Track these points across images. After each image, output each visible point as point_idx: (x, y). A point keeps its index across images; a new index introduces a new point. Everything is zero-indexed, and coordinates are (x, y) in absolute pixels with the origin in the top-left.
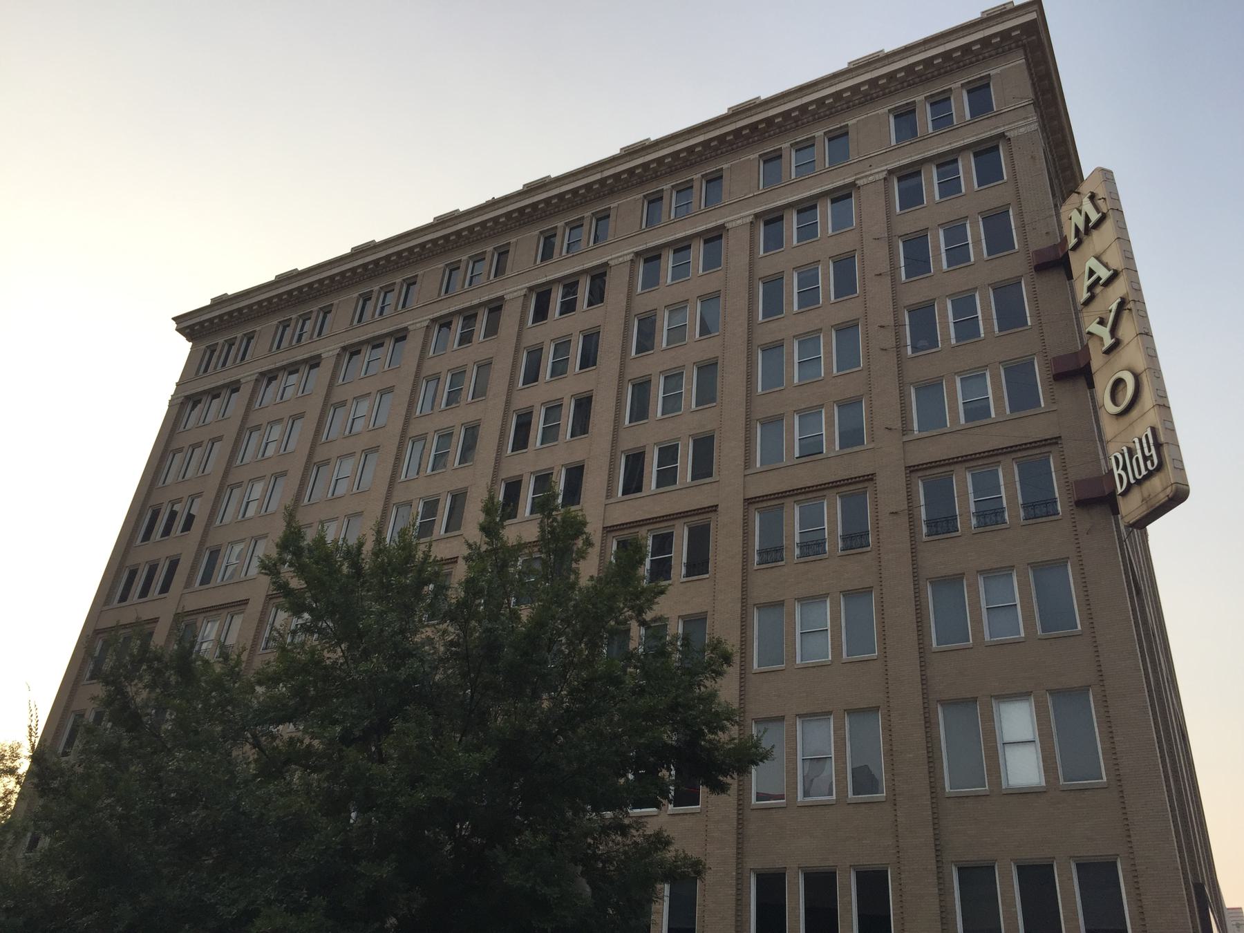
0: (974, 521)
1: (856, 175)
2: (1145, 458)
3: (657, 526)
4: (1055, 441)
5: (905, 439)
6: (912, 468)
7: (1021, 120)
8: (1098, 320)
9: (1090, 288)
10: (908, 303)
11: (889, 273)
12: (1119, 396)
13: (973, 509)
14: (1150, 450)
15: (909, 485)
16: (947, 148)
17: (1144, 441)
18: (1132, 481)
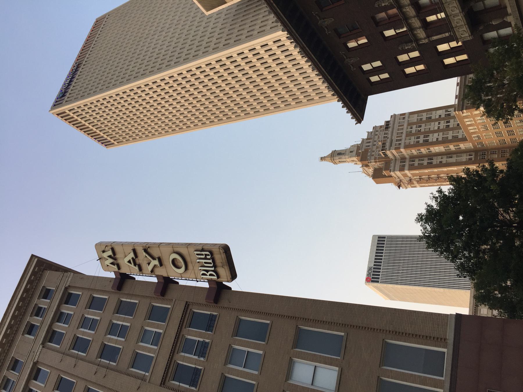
0: (202, 359)
1: (31, 360)
2: (205, 258)
4: (187, 305)
5: (148, 381)
6: (162, 383)
7: (66, 279)
8: (147, 264)
9: (135, 265)
10: (95, 356)
11: (77, 360)
12: (179, 264)
13: (196, 357)
14: (202, 255)
15: (169, 388)
16: (53, 313)
17: (199, 256)
18: (213, 269)
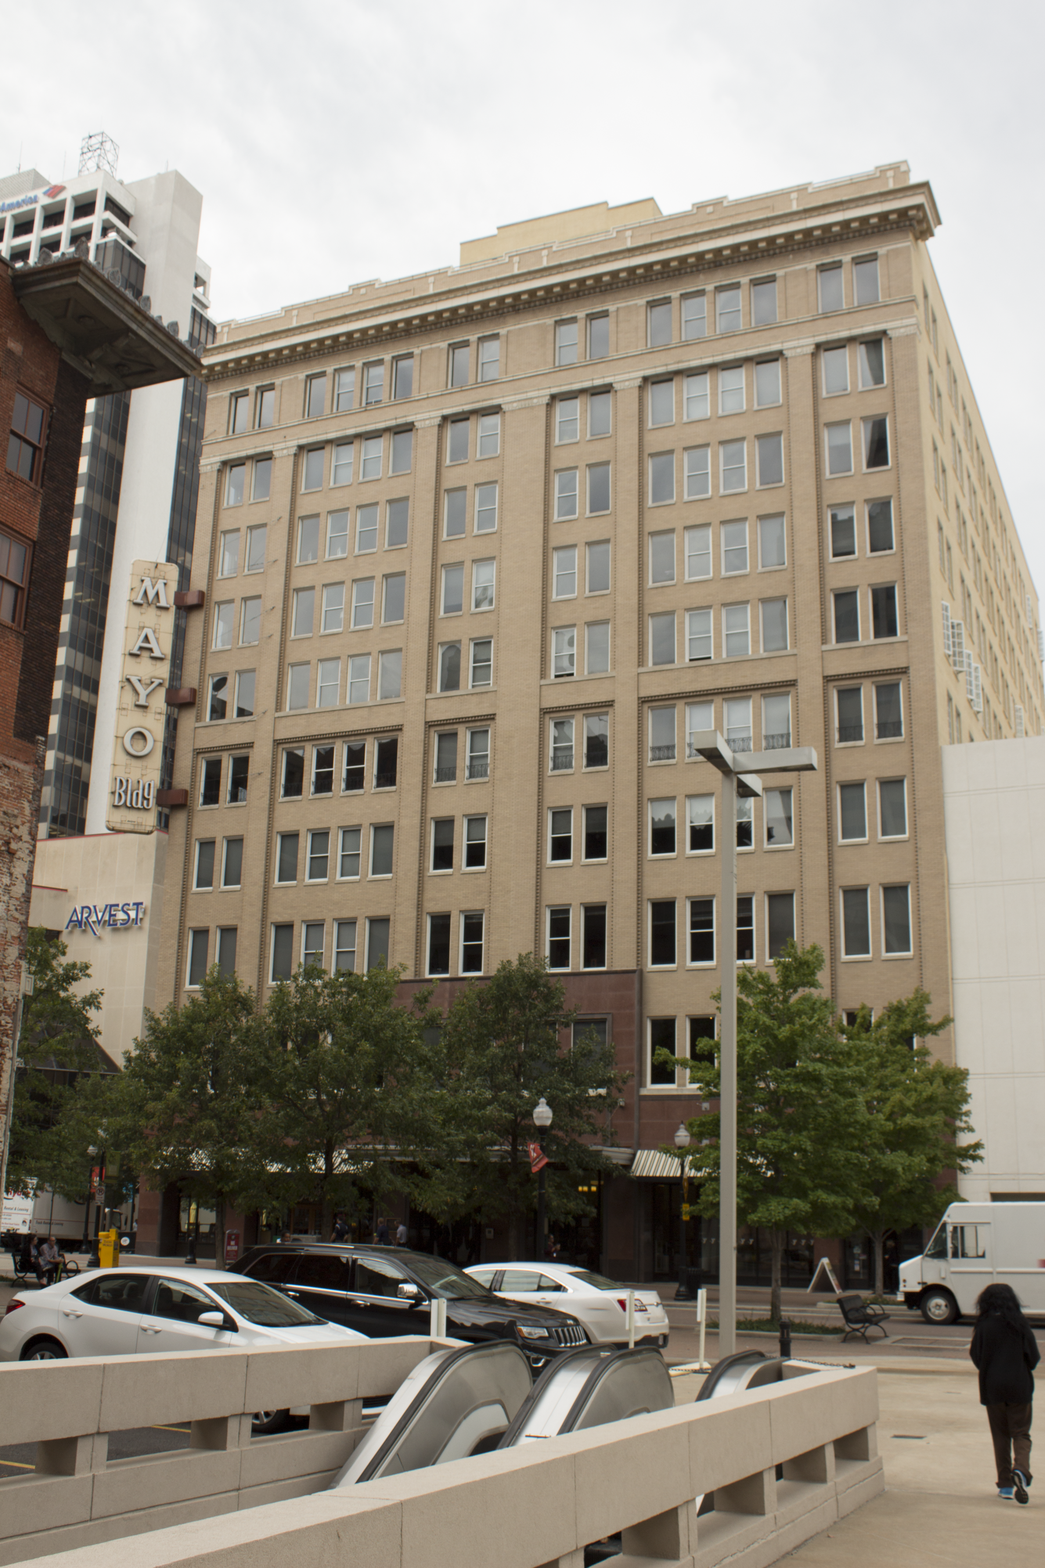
3: (353, 738)
